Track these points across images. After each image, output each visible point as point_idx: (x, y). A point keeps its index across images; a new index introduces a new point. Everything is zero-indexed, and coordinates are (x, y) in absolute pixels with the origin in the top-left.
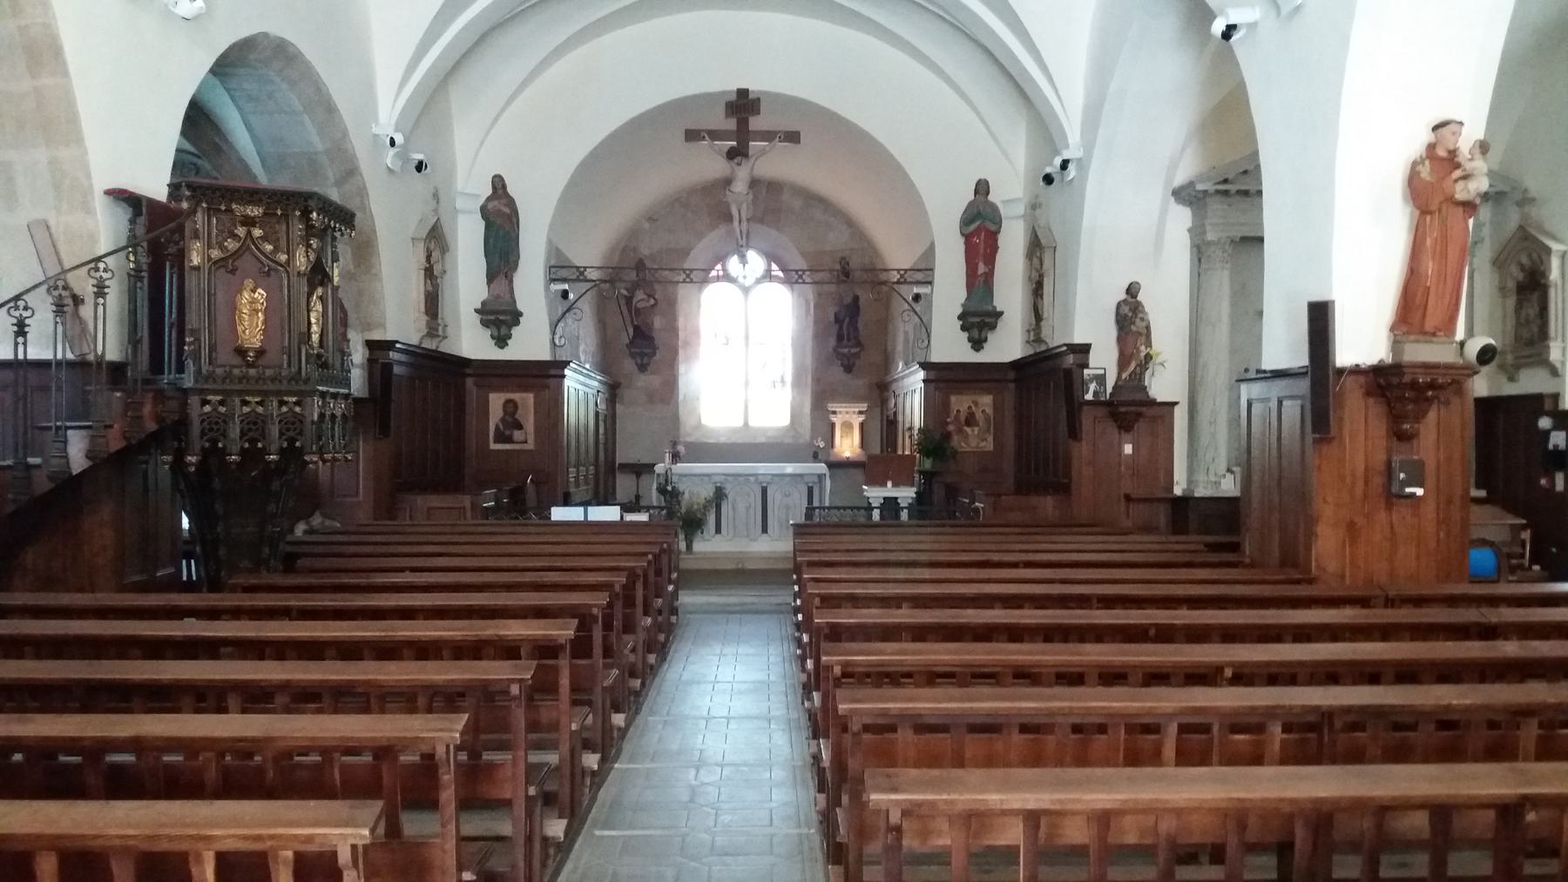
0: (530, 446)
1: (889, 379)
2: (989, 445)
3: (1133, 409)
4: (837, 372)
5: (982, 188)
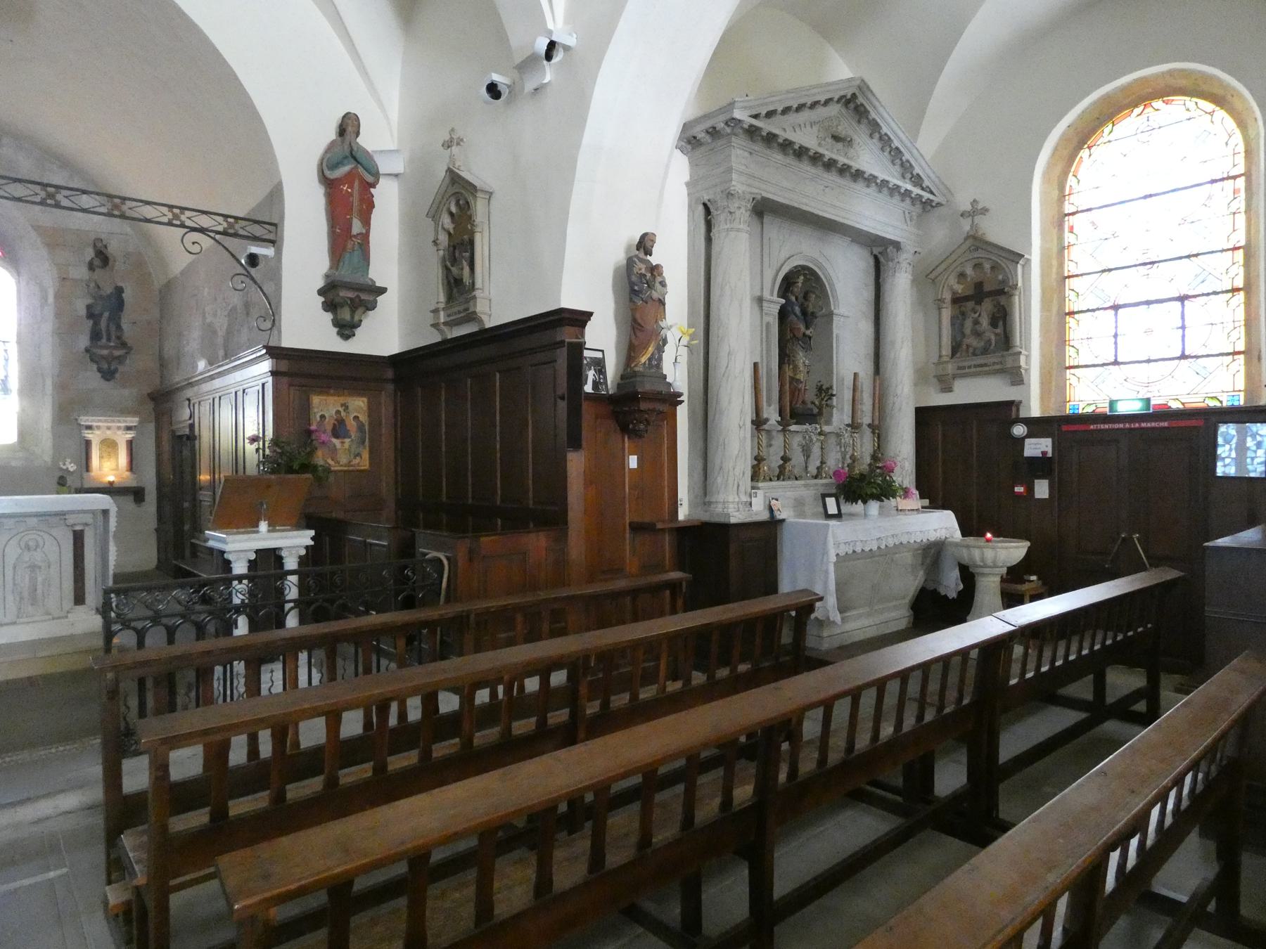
1: (178, 378)
2: (364, 462)
3: (638, 407)
4: (91, 379)
5: (348, 126)
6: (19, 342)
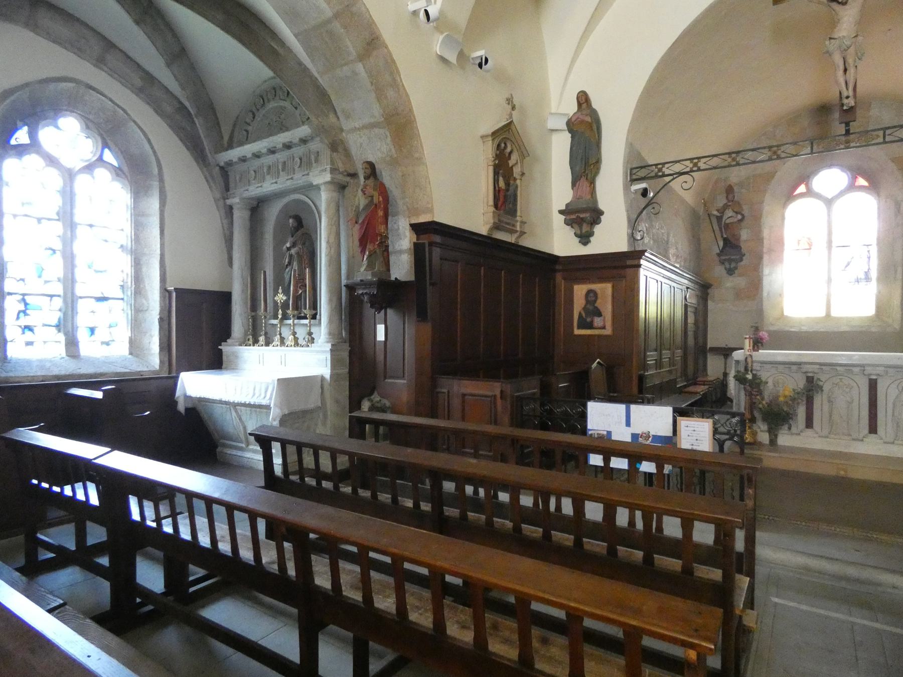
0: (608, 331)
6: (878, 244)
